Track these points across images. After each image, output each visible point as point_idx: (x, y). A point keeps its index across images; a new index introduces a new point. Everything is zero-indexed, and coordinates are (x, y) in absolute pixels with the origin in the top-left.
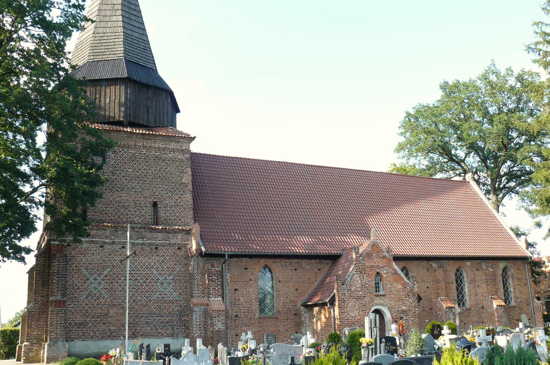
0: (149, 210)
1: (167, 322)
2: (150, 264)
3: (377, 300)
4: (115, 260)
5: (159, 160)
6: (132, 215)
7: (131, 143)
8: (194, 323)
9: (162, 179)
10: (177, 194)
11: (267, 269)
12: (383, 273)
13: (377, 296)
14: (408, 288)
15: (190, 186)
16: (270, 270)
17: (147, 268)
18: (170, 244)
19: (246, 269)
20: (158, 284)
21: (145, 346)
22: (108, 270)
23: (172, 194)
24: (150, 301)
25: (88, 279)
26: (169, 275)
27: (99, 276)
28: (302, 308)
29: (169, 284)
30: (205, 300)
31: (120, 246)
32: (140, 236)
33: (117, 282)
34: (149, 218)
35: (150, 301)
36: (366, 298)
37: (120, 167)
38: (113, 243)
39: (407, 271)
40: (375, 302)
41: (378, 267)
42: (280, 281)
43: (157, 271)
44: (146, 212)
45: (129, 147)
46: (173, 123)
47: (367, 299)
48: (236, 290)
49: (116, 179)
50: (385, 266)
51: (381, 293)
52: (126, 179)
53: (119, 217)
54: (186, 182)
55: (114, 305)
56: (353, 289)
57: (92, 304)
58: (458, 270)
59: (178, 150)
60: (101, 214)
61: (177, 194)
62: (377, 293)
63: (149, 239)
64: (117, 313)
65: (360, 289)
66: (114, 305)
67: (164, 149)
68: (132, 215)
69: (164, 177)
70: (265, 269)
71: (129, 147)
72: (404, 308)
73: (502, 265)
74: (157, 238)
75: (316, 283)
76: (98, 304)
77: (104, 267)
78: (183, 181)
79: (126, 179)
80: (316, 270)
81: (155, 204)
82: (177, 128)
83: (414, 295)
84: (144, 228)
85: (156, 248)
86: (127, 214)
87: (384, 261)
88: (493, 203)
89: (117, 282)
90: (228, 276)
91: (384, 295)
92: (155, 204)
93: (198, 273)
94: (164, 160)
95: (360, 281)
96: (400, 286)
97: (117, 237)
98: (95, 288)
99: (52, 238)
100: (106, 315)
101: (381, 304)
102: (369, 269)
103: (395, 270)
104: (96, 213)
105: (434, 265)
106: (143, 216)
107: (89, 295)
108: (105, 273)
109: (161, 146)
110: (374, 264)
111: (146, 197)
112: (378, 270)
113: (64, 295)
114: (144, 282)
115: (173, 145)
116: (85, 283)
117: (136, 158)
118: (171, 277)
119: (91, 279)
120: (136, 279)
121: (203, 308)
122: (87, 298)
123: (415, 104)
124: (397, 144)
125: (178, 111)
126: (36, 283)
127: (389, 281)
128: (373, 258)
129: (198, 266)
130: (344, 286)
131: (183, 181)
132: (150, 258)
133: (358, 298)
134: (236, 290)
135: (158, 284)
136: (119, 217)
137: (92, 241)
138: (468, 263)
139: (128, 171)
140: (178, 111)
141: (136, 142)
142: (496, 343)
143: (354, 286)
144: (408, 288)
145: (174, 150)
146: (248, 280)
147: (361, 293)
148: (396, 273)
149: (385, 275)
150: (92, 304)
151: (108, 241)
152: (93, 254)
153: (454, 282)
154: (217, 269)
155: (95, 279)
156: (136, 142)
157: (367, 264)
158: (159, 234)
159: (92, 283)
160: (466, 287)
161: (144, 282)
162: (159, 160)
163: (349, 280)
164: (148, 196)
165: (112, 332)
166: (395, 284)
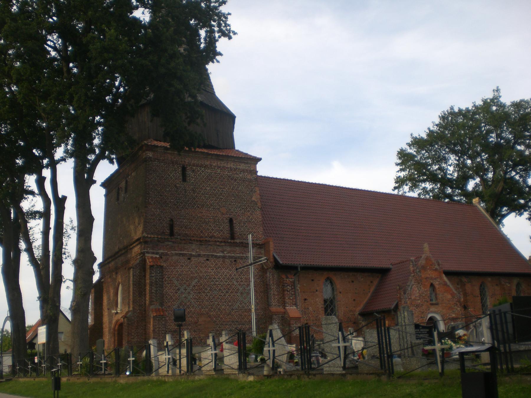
0: (227, 226)
2: (230, 275)
3: (433, 309)
4: (201, 272)
5: (232, 179)
6: (213, 230)
7: (208, 163)
9: (235, 197)
10: (249, 211)
11: (329, 282)
12: (436, 283)
13: (432, 304)
15: (259, 204)
16: (331, 282)
17: (228, 279)
19: (313, 280)
20: (239, 294)
21: (497, 312)
22: (196, 280)
23: (245, 211)
24: (233, 310)
25: (179, 289)
27: (189, 285)
28: (359, 317)
30: (281, 309)
31: (205, 259)
33: (204, 292)
34: (227, 234)
35: (233, 310)
37: (199, 186)
38: (199, 255)
40: (431, 310)
41: (432, 279)
42: (340, 293)
43: (237, 282)
44: (223, 228)
45: (206, 167)
48: (305, 299)
49: (196, 196)
51: (434, 302)
52: (205, 197)
54: (256, 200)
56: (413, 298)
58: (481, 286)
59: (247, 170)
60: (186, 228)
61: (249, 211)
62: (431, 302)
63: (229, 252)
65: (418, 298)
68: (213, 230)
69: (237, 195)
70: (326, 280)
71: (206, 167)
72: (454, 315)
73: (515, 281)
75: (369, 295)
77: (192, 278)
78: (253, 199)
79: (205, 197)
81: (231, 221)
83: (461, 305)
84: (225, 242)
85: (235, 261)
86: (208, 230)
89: (204, 292)
90: (298, 287)
92: (231, 221)
93: (273, 283)
94: (236, 180)
96: (449, 296)
98: (185, 297)
99: (146, 251)
100: (196, 323)
101: (435, 312)
103: (444, 282)
104: (181, 227)
105: (464, 279)
106: (222, 231)
107: (181, 304)
108: (193, 283)
110: (428, 276)
112: (432, 281)
113: (162, 304)
114: (227, 292)
116: (176, 293)
117: (212, 177)
119: (182, 290)
120: (220, 290)
121: (280, 316)
123: (522, 98)
126: (134, 294)
129: (273, 277)
130: (406, 296)
131: (253, 199)
132: (230, 270)
134: (305, 299)
135: (239, 294)
136: (202, 232)
137: (181, 254)
138: (489, 279)
139: (206, 189)
141: (211, 162)
145: (243, 171)
147: (419, 301)
148: (446, 284)
151: (194, 253)
152: (182, 266)
153: (479, 295)
154: (291, 280)
155: (185, 290)
156: (211, 162)
157: (423, 276)
158: (237, 248)
160: (488, 300)
161: (227, 292)
163: (409, 289)
165: (202, 340)
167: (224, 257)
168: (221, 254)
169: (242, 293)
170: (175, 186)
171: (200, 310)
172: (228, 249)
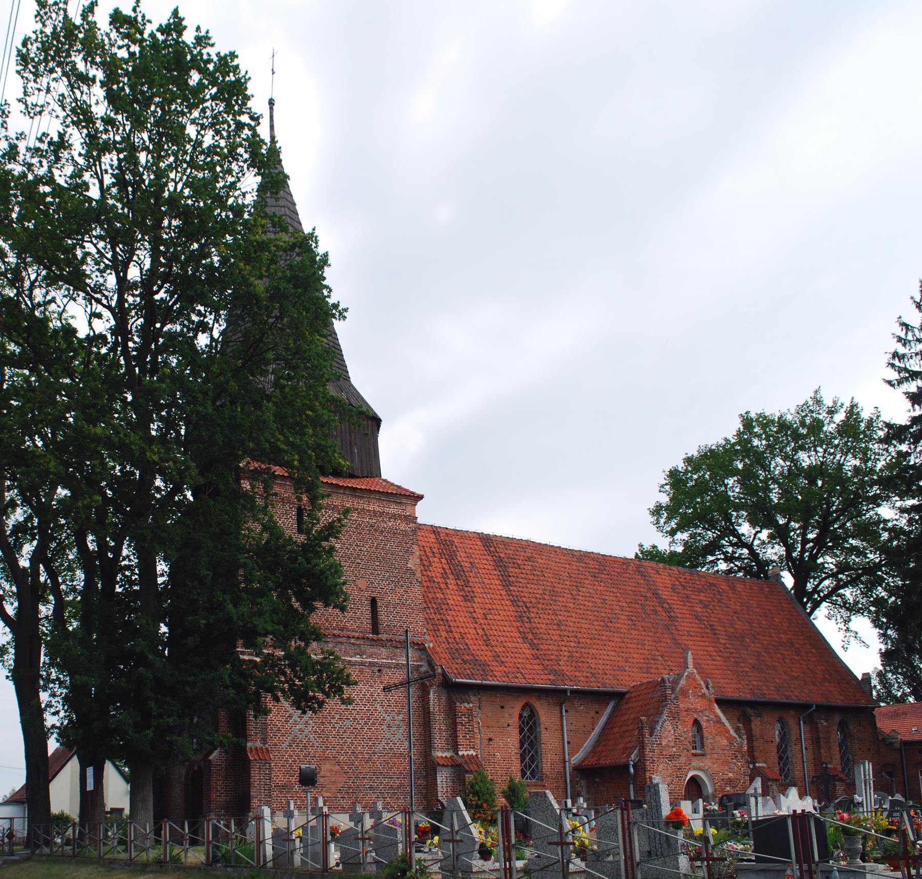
1: (398, 788)
2: (372, 695)
8: (439, 789)
13: (695, 755)
18: (398, 664)
19: (502, 707)
20: (384, 727)
25: (290, 717)
26: (398, 714)
29: (399, 727)
32: (358, 651)
34: (367, 624)
39: (531, 711)
40: (693, 764)
43: (382, 706)
46: (369, 461)
47: (683, 759)
48: (490, 740)
53: (327, 620)
55: (327, 759)
56: (664, 743)
57: (298, 756)
59: (400, 516)
63: (370, 656)
64: (331, 771)
65: (672, 744)
66: (327, 759)
67: (381, 514)
72: (731, 775)
76: (306, 756)
80: (592, 714)
81: (373, 602)
82: (385, 475)
84: (363, 638)
85: (379, 670)
88: (99, 30)
92: (373, 602)
93: (439, 710)
94: (382, 532)
95: (672, 732)
96: (725, 742)
101: (700, 769)
102: (684, 714)
103: (717, 716)
107: (294, 741)
109: (378, 509)
111: (360, 590)
112: (695, 716)
113: (264, 741)
114: (366, 723)
115: (393, 509)
118: (400, 717)
120: (355, 719)
122: (290, 746)
124: (662, 479)
127: (711, 733)
129: (439, 701)
131: (409, 565)
132: (371, 686)
133: (671, 757)
134: (490, 740)
135: (384, 727)
136: (327, 620)
143: (665, 738)
145: (394, 517)
146: (506, 725)
147: (674, 749)
148: (719, 721)
150: (298, 756)
159: (296, 723)
162: (375, 530)
164: (363, 588)
166: (718, 738)
167: (362, 664)
168: (357, 659)
169: (389, 726)
171: (324, 752)
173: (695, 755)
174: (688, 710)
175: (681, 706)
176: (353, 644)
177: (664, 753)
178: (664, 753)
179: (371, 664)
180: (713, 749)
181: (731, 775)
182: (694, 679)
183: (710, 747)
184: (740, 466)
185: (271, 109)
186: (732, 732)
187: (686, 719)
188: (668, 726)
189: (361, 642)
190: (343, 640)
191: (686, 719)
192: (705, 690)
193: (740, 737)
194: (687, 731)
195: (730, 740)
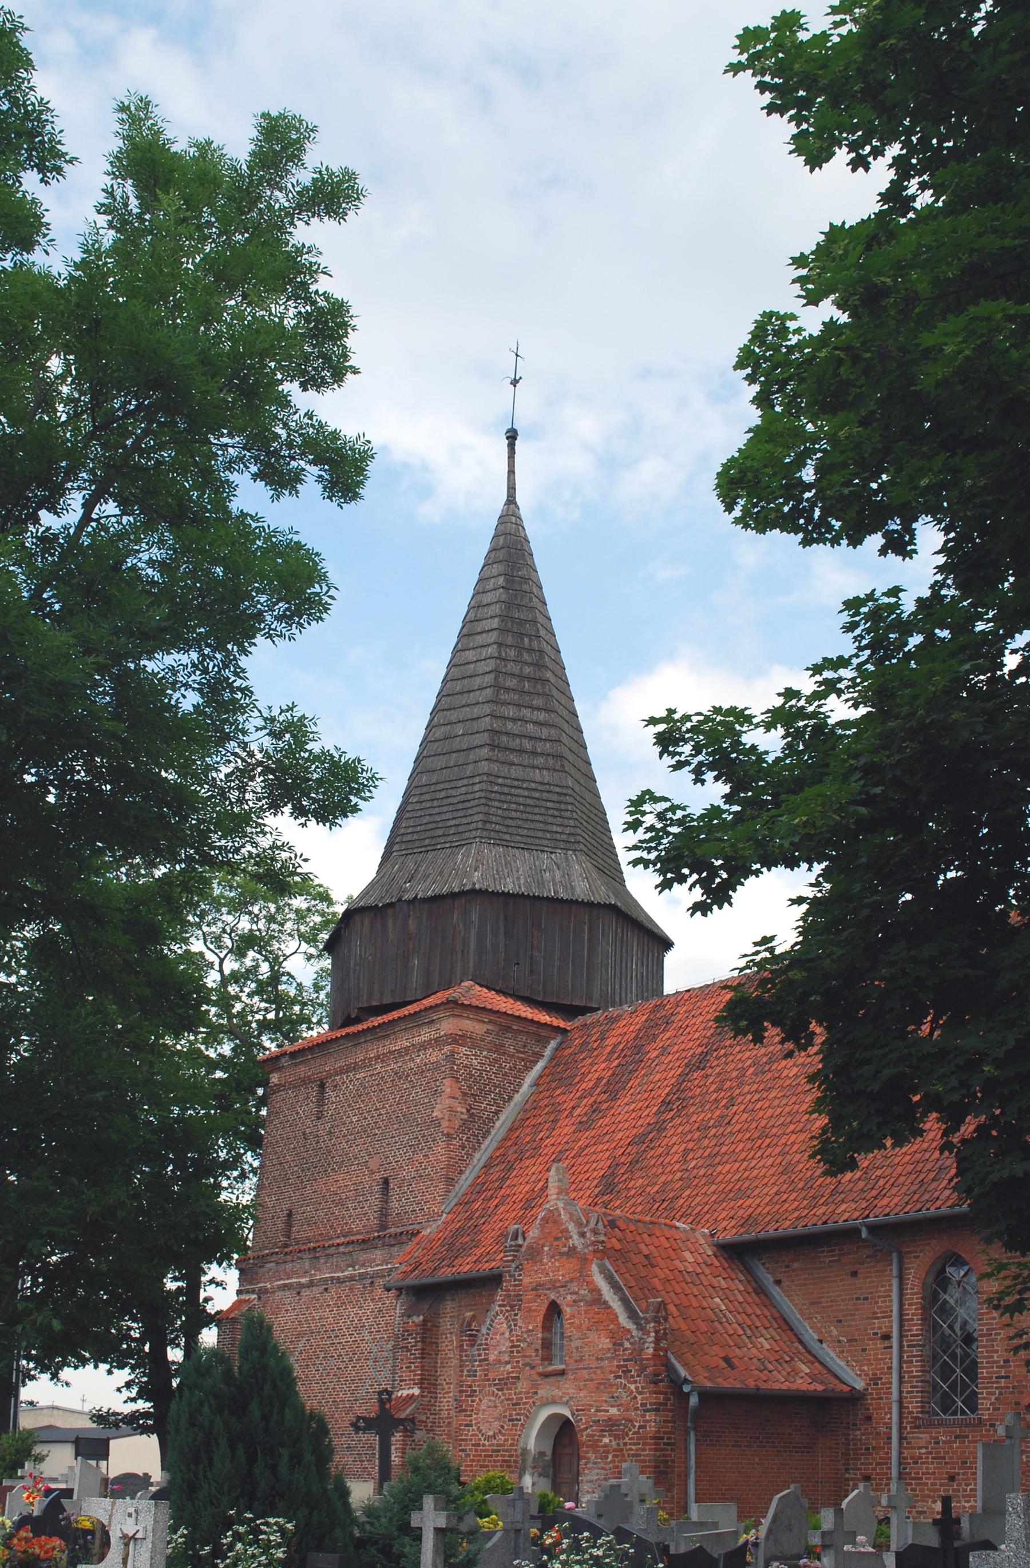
5: (400, 1078)
13: (546, 1375)
14: (627, 1345)
32: (349, 1262)
36: (519, 1385)
40: (542, 1393)
41: (554, 1286)
47: (522, 1386)
50: (572, 1280)
56: (492, 1357)
63: (363, 1265)
65: (506, 1358)
71: (355, 1067)
72: (613, 1411)
74: (374, 1260)
87: (572, 1265)
91: (562, 1373)
95: (507, 1334)
96: (605, 1342)
97: (319, 1270)
101: (553, 1402)
102: (530, 1295)
103: (596, 1291)
111: (372, 1172)
112: (552, 1297)
125: (667, 944)
127: (579, 1328)
128: (541, 1261)
133: (504, 1383)
137: (285, 1285)
140: (667, 944)
142: (174, 1529)
143: (495, 1347)
144: (627, 1345)
147: (509, 1367)
149: (568, 1310)
164: (375, 1169)
166: (592, 1336)
167: (351, 1278)
170: (304, 1134)
172: (363, 1256)
173: (546, 1375)
174: (539, 1285)
175: (526, 1280)
176: (344, 1253)
177: (491, 1376)
178: (491, 1376)
179: (363, 1277)
180: (581, 1360)
181: (613, 1411)
182: (557, 1222)
183: (576, 1356)
184: (953, 592)
185: (511, 447)
186: (623, 1319)
187: (534, 1306)
188: (501, 1324)
189: (350, 1248)
190: (332, 1250)
191: (534, 1306)
192: (576, 1241)
193: (640, 1328)
194: (531, 1326)
195: (617, 1336)
